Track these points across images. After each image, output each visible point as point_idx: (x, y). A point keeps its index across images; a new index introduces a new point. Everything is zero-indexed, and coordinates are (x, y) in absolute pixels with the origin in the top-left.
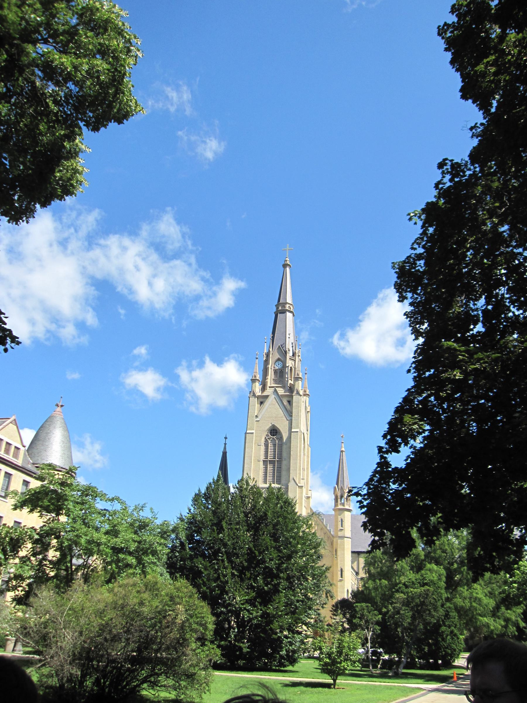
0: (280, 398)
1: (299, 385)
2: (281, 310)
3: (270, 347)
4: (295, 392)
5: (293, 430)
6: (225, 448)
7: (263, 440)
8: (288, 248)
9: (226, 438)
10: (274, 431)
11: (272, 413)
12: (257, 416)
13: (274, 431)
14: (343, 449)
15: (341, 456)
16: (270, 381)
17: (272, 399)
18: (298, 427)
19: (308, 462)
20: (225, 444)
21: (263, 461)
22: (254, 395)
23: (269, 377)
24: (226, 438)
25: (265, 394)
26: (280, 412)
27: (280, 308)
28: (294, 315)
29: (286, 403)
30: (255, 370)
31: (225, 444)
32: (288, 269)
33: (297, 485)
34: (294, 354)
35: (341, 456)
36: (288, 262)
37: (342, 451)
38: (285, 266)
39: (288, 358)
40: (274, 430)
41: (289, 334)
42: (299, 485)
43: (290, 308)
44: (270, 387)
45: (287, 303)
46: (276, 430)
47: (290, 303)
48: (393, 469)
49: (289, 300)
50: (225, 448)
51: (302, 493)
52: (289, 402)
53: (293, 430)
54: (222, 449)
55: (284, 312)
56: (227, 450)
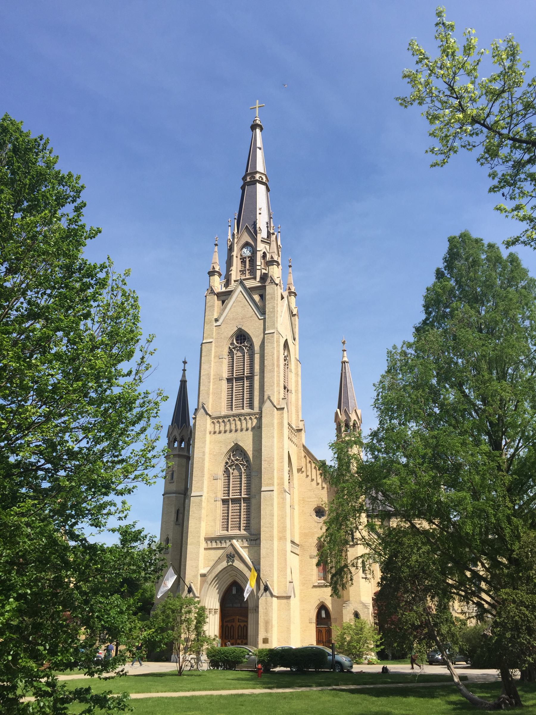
0: (250, 291)
1: (276, 272)
2: (249, 181)
3: (234, 230)
4: (269, 280)
5: (266, 332)
6: (184, 375)
7: (226, 350)
8: (257, 106)
9: (185, 362)
10: (242, 337)
11: (239, 311)
12: (216, 320)
13: (242, 337)
14: (346, 359)
15: (343, 369)
16: (235, 275)
17: (238, 292)
18: (274, 326)
19: (297, 382)
20: (184, 370)
21: (228, 379)
22: (212, 292)
23: (234, 268)
24: (185, 362)
25: (229, 289)
26: (250, 311)
27: (248, 180)
28: (268, 190)
29: (257, 298)
30: (213, 261)
31: (184, 370)
32: (258, 131)
33: (275, 406)
34: (269, 234)
35: (343, 369)
36: (258, 122)
37: (344, 362)
38: (254, 127)
39: (259, 238)
40: (241, 336)
41: (260, 209)
42: (278, 407)
43: (262, 179)
44: (235, 281)
45: (256, 172)
46: (244, 336)
47: (263, 172)
48: (456, 284)
49: (260, 167)
50: (184, 375)
51: (282, 418)
52: (262, 297)
53: (266, 332)
54: (180, 378)
55: (254, 182)
56: (187, 378)
